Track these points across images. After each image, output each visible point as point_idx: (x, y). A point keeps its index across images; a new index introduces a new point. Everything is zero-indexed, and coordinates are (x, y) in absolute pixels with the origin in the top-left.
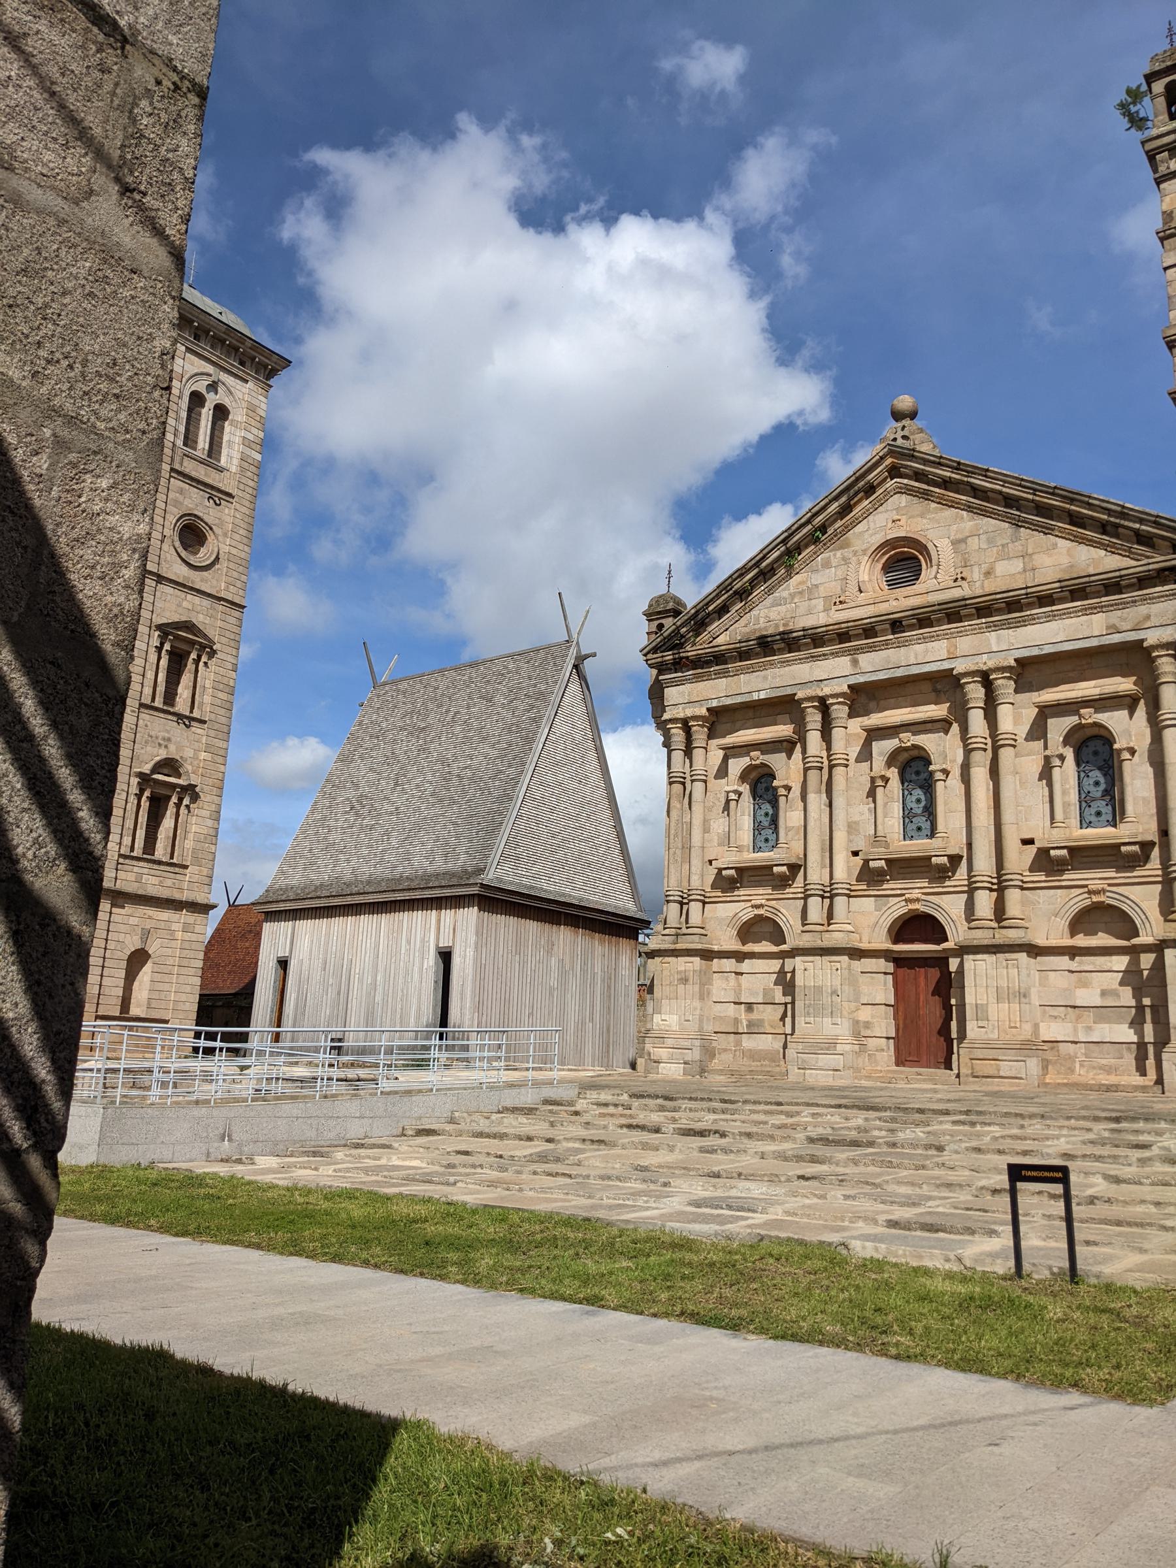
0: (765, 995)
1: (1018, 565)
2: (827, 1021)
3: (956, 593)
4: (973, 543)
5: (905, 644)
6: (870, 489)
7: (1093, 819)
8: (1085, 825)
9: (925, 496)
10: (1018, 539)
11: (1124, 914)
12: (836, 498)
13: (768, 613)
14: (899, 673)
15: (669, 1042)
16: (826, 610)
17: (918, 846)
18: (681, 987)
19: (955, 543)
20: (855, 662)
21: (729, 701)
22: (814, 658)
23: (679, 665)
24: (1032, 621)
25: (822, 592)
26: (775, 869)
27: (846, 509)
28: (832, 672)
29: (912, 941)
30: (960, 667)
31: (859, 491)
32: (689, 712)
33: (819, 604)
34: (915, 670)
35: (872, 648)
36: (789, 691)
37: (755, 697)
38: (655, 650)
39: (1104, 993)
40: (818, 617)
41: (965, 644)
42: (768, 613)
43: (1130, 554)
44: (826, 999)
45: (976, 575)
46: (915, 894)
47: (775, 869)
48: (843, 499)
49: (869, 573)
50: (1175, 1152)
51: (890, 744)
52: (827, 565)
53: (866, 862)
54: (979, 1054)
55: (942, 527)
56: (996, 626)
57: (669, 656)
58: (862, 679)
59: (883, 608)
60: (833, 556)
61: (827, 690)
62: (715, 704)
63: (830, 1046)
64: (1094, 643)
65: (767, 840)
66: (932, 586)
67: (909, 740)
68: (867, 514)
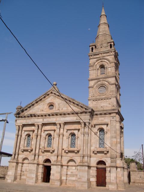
1: (66, 109)
3: (57, 112)
4: (61, 104)
6: (48, 95)
11: (73, 160)
12: (43, 95)
14: (49, 122)
16: (40, 112)
17: (102, 149)
20: (43, 120)
21: (26, 124)
22: (38, 118)
23: (19, 117)
24: (67, 117)
25: (40, 109)
26: (105, 152)
27: (45, 97)
28: (40, 121)
29: (47, 163)
31: (46, 95)
32: (19, 125)
33: (40, 111)
35: (46, 118)
36: (34, 123)
37: (29, 123)
38: (16, 114)
39: (71, 172)
40: (39, 113)
41: (58, 119)
43: (80, 109)
44: (33, 171)
45: (60, 109)
46: (47, 156)
47: (105, 152)
48: (44, 96)
50: (1, 180)
52: (41, 105)
53: (65, 151)
55: (57, 101)
57: (18, 116)
58: (44, 123)
59: (48, 112)
60: (42, 103)
61: (39, 124)
62: (23, 124)
63: (33, 178)
66: (54, 110)
67: (72, 131)
68: (59, 99)
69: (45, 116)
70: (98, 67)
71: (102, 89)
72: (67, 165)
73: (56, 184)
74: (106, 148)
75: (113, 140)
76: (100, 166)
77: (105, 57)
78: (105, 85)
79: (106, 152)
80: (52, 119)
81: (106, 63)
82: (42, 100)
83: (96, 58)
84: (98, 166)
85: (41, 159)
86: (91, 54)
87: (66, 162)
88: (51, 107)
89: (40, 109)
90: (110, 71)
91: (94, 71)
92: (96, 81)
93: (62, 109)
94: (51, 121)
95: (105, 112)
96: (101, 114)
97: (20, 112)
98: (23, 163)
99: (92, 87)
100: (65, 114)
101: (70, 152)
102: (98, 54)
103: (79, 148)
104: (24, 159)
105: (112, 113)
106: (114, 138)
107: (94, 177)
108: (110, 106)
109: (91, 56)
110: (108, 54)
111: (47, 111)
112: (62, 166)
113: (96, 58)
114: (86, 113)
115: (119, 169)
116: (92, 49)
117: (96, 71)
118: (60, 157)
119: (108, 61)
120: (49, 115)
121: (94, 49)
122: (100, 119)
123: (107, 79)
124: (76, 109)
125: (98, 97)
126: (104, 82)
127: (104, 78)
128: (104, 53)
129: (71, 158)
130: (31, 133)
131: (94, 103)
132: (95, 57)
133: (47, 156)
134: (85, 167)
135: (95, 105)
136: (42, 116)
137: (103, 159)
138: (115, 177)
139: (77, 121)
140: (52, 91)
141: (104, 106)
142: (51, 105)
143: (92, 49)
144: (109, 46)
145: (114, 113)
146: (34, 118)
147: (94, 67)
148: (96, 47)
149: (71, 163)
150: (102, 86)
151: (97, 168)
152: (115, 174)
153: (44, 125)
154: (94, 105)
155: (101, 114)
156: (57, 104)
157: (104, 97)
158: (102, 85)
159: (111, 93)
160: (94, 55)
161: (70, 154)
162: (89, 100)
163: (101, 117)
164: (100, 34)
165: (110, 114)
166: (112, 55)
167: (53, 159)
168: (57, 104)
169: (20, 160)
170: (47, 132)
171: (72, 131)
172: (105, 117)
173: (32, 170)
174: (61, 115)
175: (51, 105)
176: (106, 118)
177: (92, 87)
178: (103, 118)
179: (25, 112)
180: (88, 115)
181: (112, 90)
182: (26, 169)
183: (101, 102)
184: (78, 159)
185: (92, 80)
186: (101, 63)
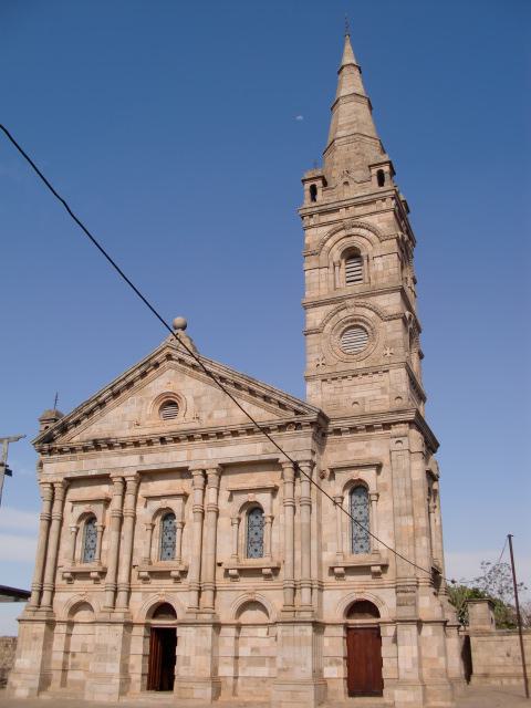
0: (82, 647)
2: (109, 664)
5: (167, 451)
6: (157, 365)
7: (360, 549)
8: (165, 556)
9: (184, 371)
10: (224, 400)
13: (97, 428)
14: (163, 467)
15: (23, 676)
17: (361, 559)
18: (33, 643)
19: (195, 398)
20: (142, 458)
23: (51, 452)
24: (229, 443)
25: (129, 418)
27: (144, 374)
30: (192, 466)
31: (150, 366)
32: (54, 479)
33: (127, 424)
34: (171, 466)
38: (39, 442)
39: (252, 650)
40: (126, 433)
41: (196, 454)
42: (97, 428)
43: (276, 412)
45: (204, 416)
46: (161, 590)
49: (150, 409)
51: (156, 505)
53: (227, 570)
54: (185, 685)
55: (191, 388)
56: (210, 446)
57: (46, 447)
58: (144, 469)
59: (157, 430)
61: (125, 474)
63: (111, 677)
64: (257, 458)
65: (362, 547)
67: (250, 497)
68: (198, 378)
69: (149, 442)
70: (336, 255)
71: (355, 335)
72: (235, 622)
73: (198, 693)
74: (377, 552)
75: (403, 524)
76: (358, 621)
77: (361, 220)
78: (365, 323)
79: (378, 568)
80: (174, 453)
81: (364, 240)
82: (136, 384)
83: (329, 223)
84: (350, 621)
85: (140, 605)
86: (308, 211)
87: (233, 610)
88: (170, 410)
89: (129, 418)
90: (380, 268)
91: (323, 271)
92: (331, 307)
93: (210, 416)
94: (170, 461)
95: (369, 421)
96: (353, 429)
97: (55, 432)
98: (71, 624)
99: (318, 332)
100: (220, 435)
101: (244, 572)
102: (337, 210)
103: (277, 558)
104: (75, 608)
105: (395, 424)
106: (407, 514)
107: (338, 663)
108: (387, 397)
109: (311, 216)
110: (372, 208)
111: (154, 425)
112: (217, 626)
113: (329, 223)
114: (298, 426)
115: (427, 630)
116: (313, 190)
117: (331, 271)
118: (207, 595)
119: (372, 235)
120: (163, 440)
121: (319, 191)
122: (350, 449)
123: (372, 301)
124: (262, 414)
125: (342, 367)
126: (360, 311)
127: (360, 297)
128: (357, 205)
129: (250, 597)
130: (98, 509)
131: (327, 388)
132: (324, 219)
133: (161, 590)
134: (303, 627)
135: (331, 394)
136: (136, 444)
137: (369, 596)
138: (413, 659)
139: (266, 457)
140: (171, 351)
141: (364, 399)
142: (169, 403)
143: (313, 190)
144: (375, 179)
145: (402, 422)
146: (108, 451)
147: (323, 256)
148: (325, 184)
149: (251, 616)
150: (355, 325)
151: (348, 628)
152: (415, 648)
153: (145, 476)
154: (328, 398)
155: (353, 429)
156: (190, 399)
157: (362, 365)
158: (356, 320)
159: (388, 352)
160: (322, 213)
161: (247, 583)
162: (307, 379)
163: (355, 440)
164: (340, 134)
165: (387, 426)
166: (385, 211)
167: (183, 601)
168: (190, 399)
169: (61, 613)
170: (156, 505)
171: (163, 501)
172: (370, 438)
173: (106, 646)
174: (205, 436)
175: (169, 403)
176: (373, 442)
177: (318, 332)
178: (360, 445)
179: (72, 431)
180: (306, 435)
181: (391, 337)
182: (84, 645)
183: (350, 383)
184: (275, 599)
185: (316, 305)
186: (347, 243)
